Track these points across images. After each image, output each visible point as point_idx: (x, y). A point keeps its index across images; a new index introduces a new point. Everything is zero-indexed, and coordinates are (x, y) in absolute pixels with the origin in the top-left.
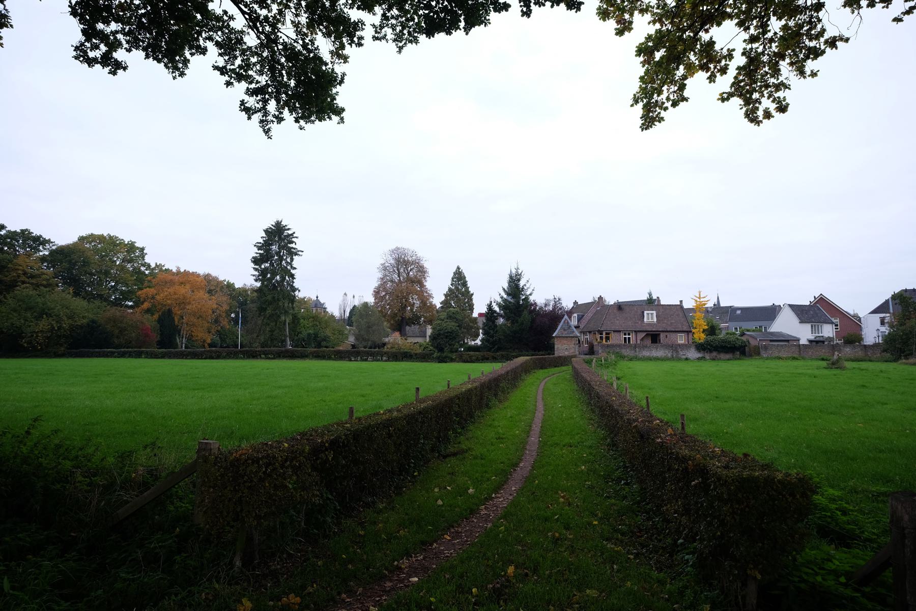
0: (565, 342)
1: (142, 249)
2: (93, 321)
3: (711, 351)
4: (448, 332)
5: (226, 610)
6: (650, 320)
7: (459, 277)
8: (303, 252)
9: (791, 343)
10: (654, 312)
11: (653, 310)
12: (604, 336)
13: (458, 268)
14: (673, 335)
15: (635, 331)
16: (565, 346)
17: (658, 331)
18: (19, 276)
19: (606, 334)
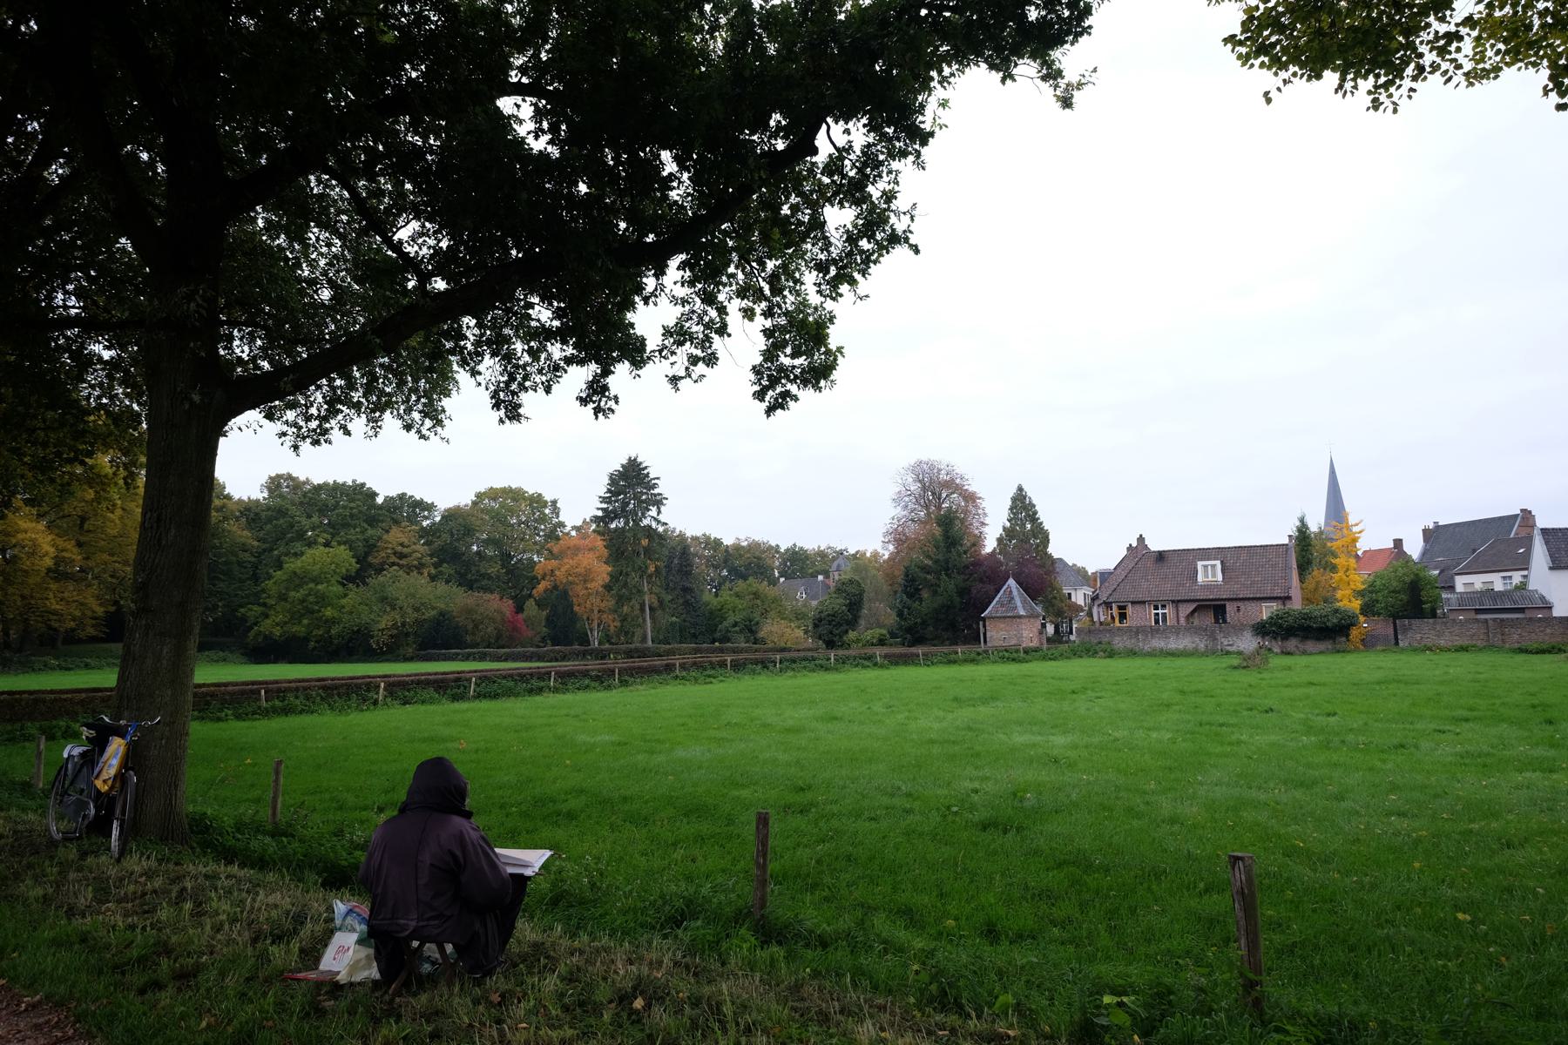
0: (1003, 626)
1: (554, 502)
2: (442, 614)
3: (1285, 638)
4: (829, 615)
5: (992, 1044)
6: (1210, 579)
7: (1022, 506)
8: (658, 478)
9: (1529, 614)
10: (1218, 563)
11: (1215, 559)
12: (1115, 611)
13: (1020, 489)
14: (1251, 606)
15: (1173, 601)
16: (1003, 634)
17: (1222, 600)
18: (388, 557)
19: (1120, 608)
